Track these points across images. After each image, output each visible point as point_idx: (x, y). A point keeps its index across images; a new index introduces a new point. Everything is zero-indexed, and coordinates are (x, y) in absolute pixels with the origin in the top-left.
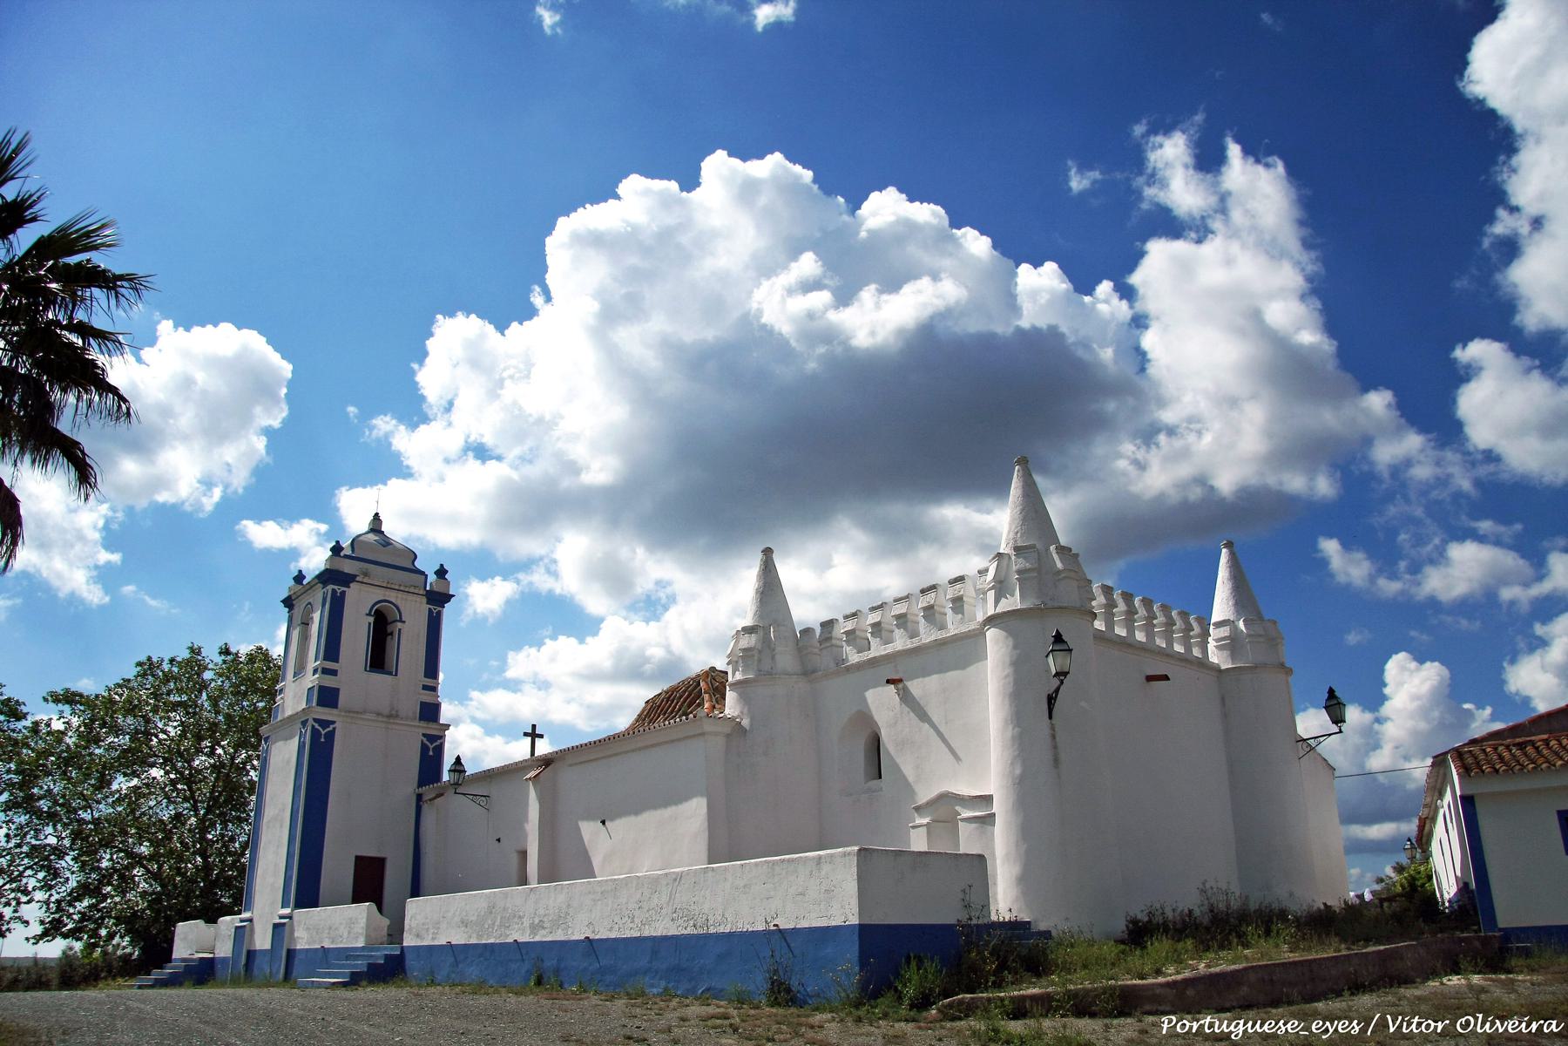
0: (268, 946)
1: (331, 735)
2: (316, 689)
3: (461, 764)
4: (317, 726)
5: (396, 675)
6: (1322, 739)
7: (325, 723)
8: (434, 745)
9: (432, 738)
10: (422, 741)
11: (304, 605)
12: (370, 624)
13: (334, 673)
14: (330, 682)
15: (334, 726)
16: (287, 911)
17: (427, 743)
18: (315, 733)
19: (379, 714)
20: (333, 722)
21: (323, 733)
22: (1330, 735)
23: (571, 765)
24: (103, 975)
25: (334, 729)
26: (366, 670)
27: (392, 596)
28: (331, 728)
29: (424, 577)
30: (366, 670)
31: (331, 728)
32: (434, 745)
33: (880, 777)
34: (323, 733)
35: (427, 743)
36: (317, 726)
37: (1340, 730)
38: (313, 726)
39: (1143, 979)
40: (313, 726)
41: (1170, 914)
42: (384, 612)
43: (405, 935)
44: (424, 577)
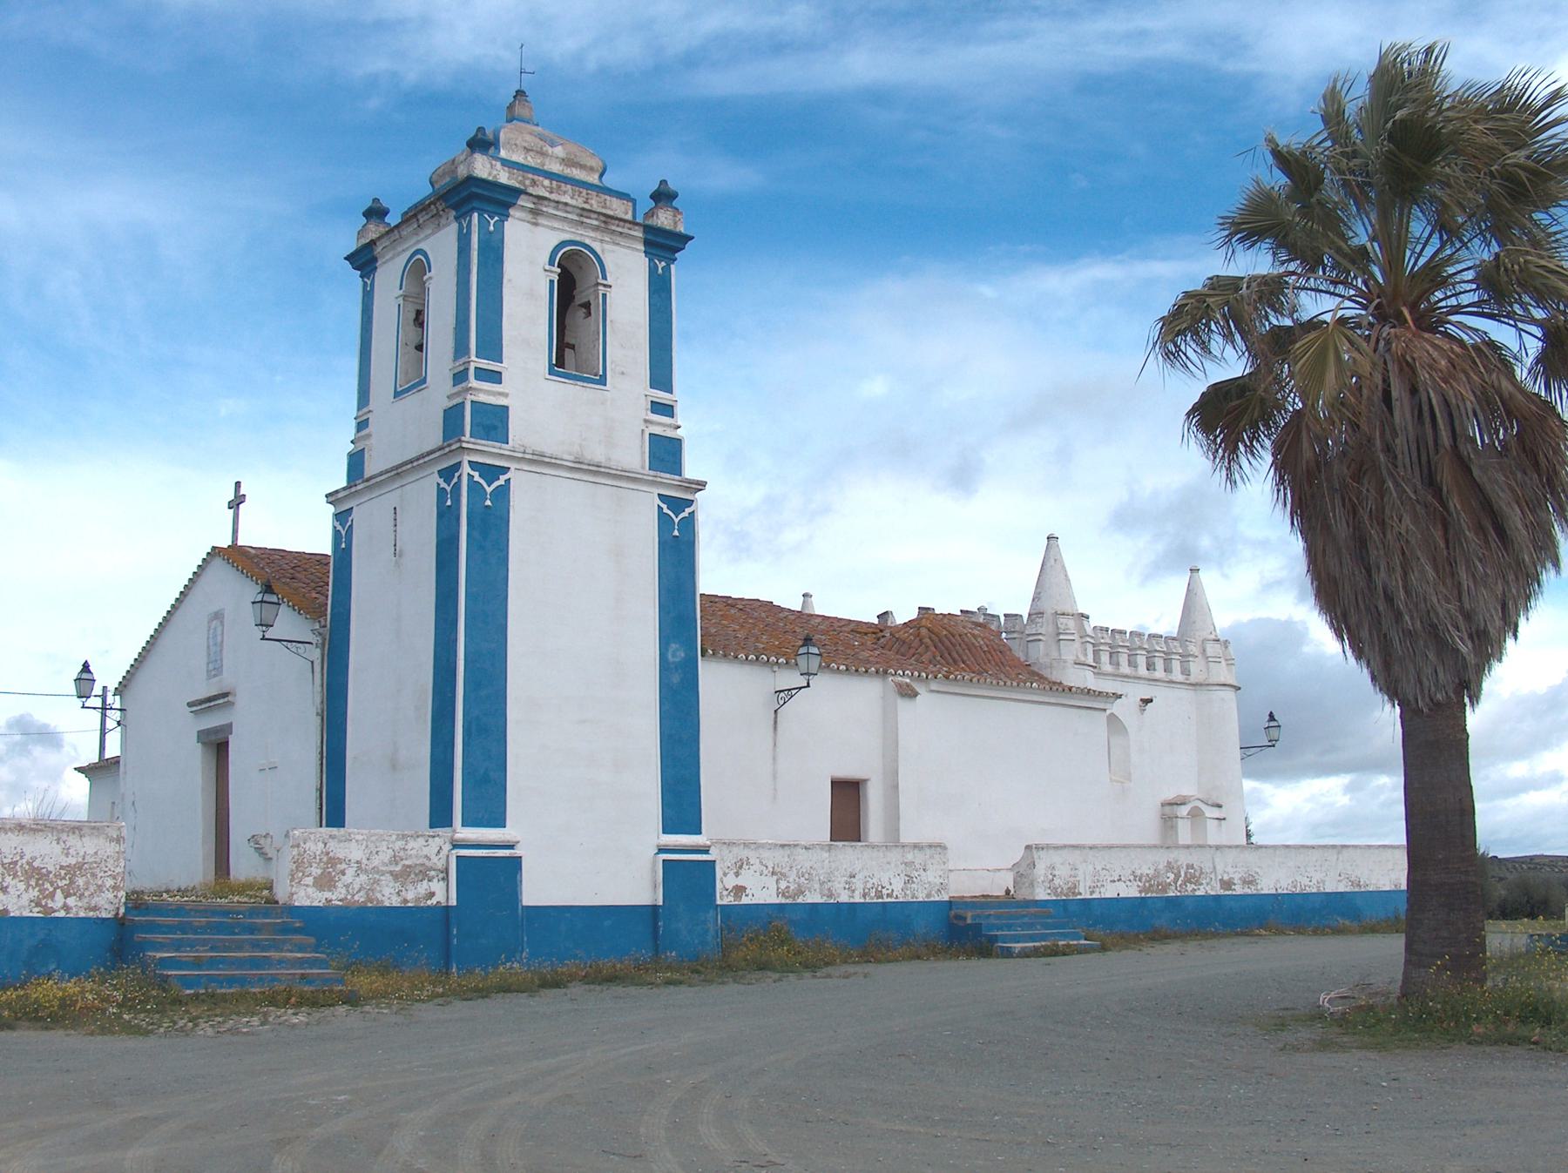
0: (455, 904)
1: (503, 493)
3: (90, 672)
4: (476, 475)
6: (794, 692)
8: (682, 515)
9: (678, 504)
11: (408, 254)
12: (552, 282)
13: (496, 377)
17: (482, 481)
20: (506, 470)
21: (489, 490)
22: (800, 688)
24: (1476, 1028)
25: (508, 481)
27: (589, 238)
28: (501, 482)
31: (501, 482)
34: (489, 490)
35: (482, 481)
36: (477, 478)
37: (808, 683)
39: (252, 933)
43: (1339, 890)
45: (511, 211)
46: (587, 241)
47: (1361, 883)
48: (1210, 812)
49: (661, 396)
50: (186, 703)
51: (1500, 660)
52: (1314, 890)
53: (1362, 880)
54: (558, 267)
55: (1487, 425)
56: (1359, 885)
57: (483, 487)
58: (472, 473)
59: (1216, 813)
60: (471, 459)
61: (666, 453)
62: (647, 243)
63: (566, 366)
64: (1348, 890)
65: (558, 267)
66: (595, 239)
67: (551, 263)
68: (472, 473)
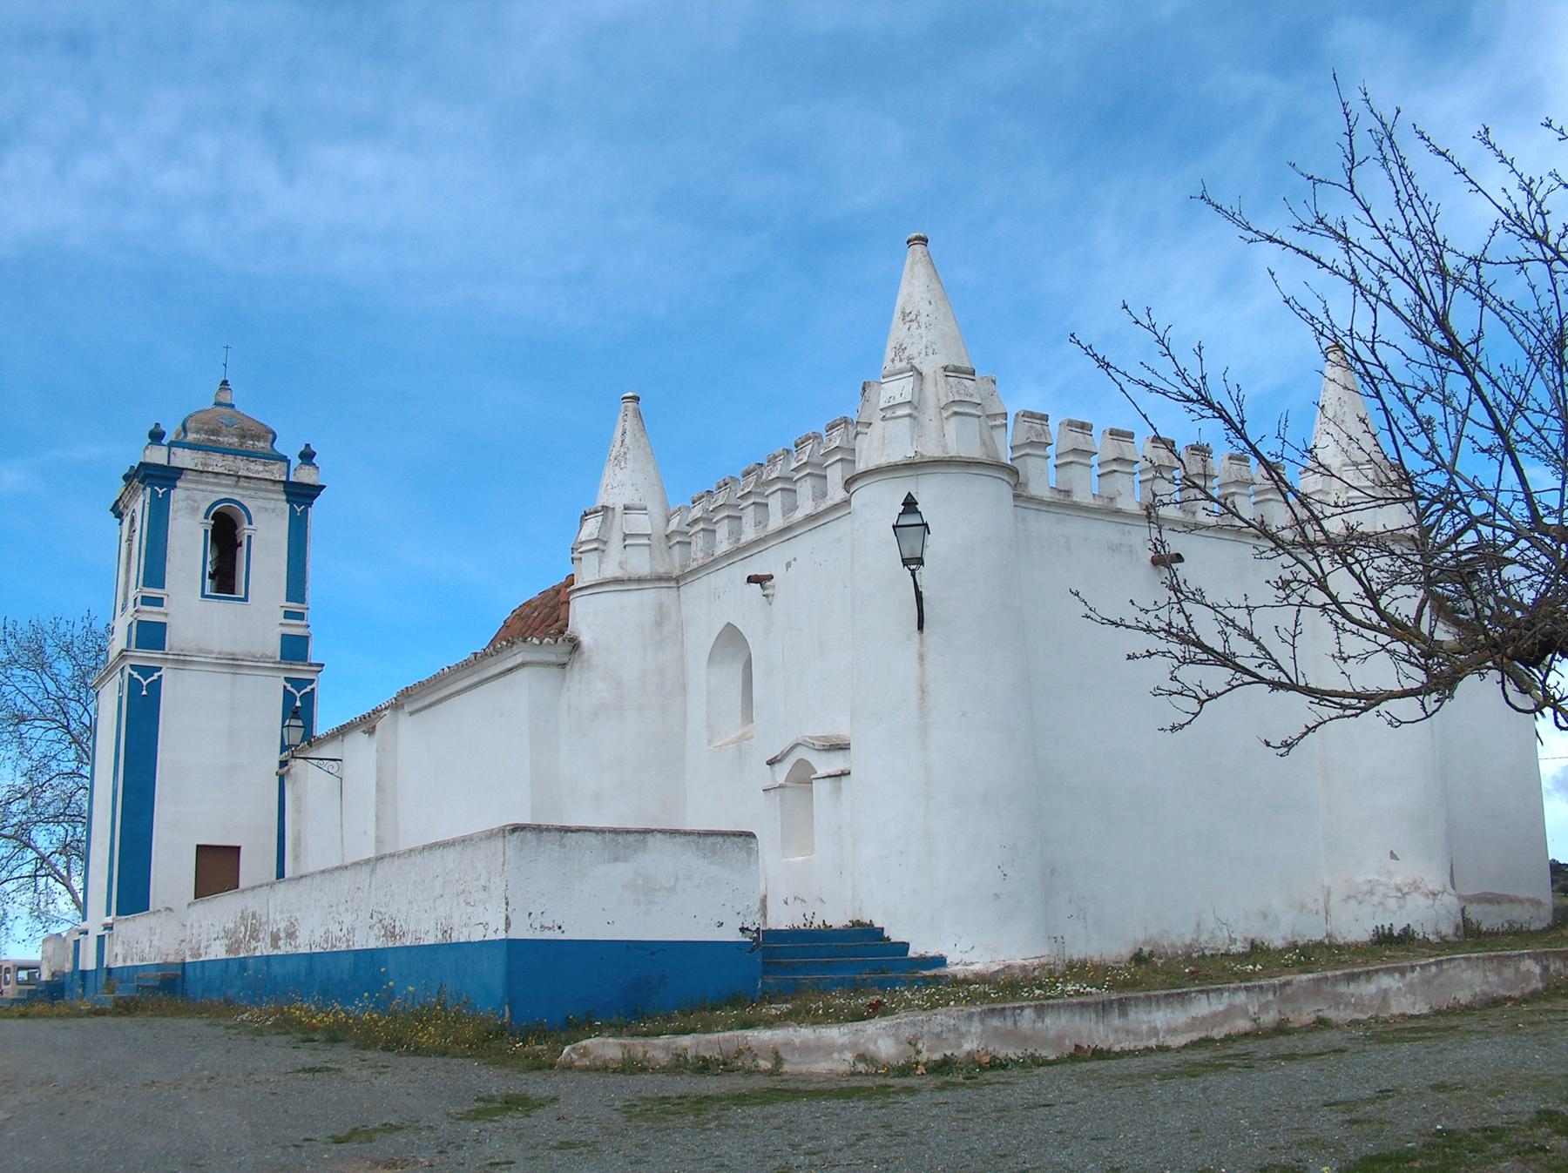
0: (93, 967)
1: (156, 687)
2: (135, 625)
4: (136, 675)
5: (246, 599)
7: (146, 671)
8: (302, 692)
9: (298, 683)
10: (285, 687)
12: (206, 531)
13: (158, 602)
14: (151, 615)
15: (159, 674)
16: (109, 920)
17: (292, 690)
18: (134, 685)
19: (921, 657)
21: (145, 683)
23: (411, 714)
25: (160, 677)
26: (204, 596)
28: (308, 689)
29: (286, 464)
30: (204, 596)
32: (302, 692)
33: (751, 835)
34: (145, 683)
35: (292, 690)
36: (136, 675)
38: (130, 675)
40: (130, 675)
41: (1093, 1016)
42: (225, 511)
44: (286, 464)
45: (178, 484)
46: (237, 498)
47: (397, 931)
48: (826, 764)
49: (294, 606)
50: (765, 763)
51: (132, 467)
52: (344, 947)
53: (397, 924)
54: (212, 519)
55: (1024, 1001)
56: (393, 935)
57: (140, 681)
58: (132, 672)
59: (835, 763)
60: (133, 663)
61: (295, 649)
62: (286, 492)
63: (236, 592)
64: (380, 944)
65: (212, 519)
66: (243, 496)
67: (206, 517)
68: (132, 672)
